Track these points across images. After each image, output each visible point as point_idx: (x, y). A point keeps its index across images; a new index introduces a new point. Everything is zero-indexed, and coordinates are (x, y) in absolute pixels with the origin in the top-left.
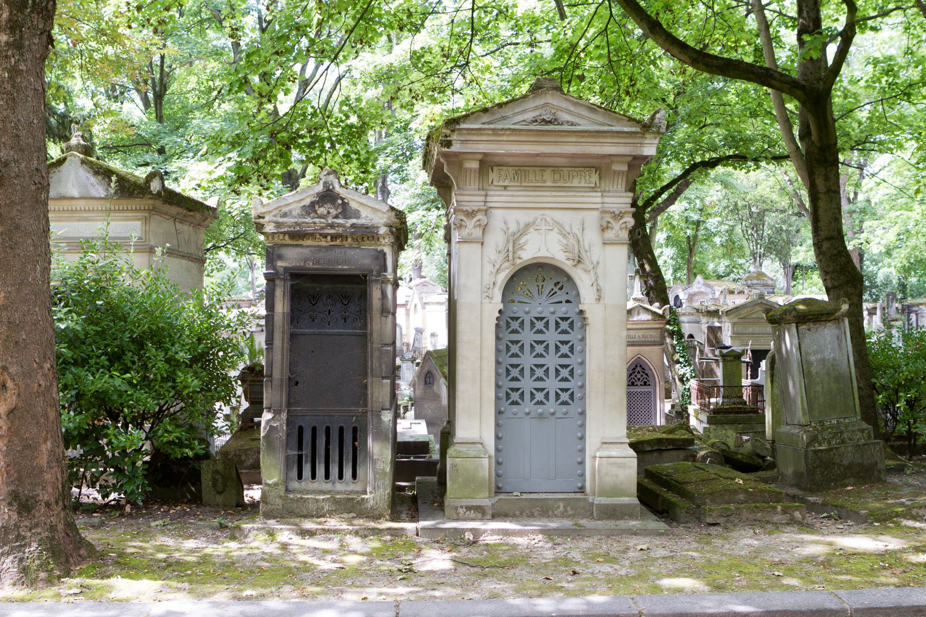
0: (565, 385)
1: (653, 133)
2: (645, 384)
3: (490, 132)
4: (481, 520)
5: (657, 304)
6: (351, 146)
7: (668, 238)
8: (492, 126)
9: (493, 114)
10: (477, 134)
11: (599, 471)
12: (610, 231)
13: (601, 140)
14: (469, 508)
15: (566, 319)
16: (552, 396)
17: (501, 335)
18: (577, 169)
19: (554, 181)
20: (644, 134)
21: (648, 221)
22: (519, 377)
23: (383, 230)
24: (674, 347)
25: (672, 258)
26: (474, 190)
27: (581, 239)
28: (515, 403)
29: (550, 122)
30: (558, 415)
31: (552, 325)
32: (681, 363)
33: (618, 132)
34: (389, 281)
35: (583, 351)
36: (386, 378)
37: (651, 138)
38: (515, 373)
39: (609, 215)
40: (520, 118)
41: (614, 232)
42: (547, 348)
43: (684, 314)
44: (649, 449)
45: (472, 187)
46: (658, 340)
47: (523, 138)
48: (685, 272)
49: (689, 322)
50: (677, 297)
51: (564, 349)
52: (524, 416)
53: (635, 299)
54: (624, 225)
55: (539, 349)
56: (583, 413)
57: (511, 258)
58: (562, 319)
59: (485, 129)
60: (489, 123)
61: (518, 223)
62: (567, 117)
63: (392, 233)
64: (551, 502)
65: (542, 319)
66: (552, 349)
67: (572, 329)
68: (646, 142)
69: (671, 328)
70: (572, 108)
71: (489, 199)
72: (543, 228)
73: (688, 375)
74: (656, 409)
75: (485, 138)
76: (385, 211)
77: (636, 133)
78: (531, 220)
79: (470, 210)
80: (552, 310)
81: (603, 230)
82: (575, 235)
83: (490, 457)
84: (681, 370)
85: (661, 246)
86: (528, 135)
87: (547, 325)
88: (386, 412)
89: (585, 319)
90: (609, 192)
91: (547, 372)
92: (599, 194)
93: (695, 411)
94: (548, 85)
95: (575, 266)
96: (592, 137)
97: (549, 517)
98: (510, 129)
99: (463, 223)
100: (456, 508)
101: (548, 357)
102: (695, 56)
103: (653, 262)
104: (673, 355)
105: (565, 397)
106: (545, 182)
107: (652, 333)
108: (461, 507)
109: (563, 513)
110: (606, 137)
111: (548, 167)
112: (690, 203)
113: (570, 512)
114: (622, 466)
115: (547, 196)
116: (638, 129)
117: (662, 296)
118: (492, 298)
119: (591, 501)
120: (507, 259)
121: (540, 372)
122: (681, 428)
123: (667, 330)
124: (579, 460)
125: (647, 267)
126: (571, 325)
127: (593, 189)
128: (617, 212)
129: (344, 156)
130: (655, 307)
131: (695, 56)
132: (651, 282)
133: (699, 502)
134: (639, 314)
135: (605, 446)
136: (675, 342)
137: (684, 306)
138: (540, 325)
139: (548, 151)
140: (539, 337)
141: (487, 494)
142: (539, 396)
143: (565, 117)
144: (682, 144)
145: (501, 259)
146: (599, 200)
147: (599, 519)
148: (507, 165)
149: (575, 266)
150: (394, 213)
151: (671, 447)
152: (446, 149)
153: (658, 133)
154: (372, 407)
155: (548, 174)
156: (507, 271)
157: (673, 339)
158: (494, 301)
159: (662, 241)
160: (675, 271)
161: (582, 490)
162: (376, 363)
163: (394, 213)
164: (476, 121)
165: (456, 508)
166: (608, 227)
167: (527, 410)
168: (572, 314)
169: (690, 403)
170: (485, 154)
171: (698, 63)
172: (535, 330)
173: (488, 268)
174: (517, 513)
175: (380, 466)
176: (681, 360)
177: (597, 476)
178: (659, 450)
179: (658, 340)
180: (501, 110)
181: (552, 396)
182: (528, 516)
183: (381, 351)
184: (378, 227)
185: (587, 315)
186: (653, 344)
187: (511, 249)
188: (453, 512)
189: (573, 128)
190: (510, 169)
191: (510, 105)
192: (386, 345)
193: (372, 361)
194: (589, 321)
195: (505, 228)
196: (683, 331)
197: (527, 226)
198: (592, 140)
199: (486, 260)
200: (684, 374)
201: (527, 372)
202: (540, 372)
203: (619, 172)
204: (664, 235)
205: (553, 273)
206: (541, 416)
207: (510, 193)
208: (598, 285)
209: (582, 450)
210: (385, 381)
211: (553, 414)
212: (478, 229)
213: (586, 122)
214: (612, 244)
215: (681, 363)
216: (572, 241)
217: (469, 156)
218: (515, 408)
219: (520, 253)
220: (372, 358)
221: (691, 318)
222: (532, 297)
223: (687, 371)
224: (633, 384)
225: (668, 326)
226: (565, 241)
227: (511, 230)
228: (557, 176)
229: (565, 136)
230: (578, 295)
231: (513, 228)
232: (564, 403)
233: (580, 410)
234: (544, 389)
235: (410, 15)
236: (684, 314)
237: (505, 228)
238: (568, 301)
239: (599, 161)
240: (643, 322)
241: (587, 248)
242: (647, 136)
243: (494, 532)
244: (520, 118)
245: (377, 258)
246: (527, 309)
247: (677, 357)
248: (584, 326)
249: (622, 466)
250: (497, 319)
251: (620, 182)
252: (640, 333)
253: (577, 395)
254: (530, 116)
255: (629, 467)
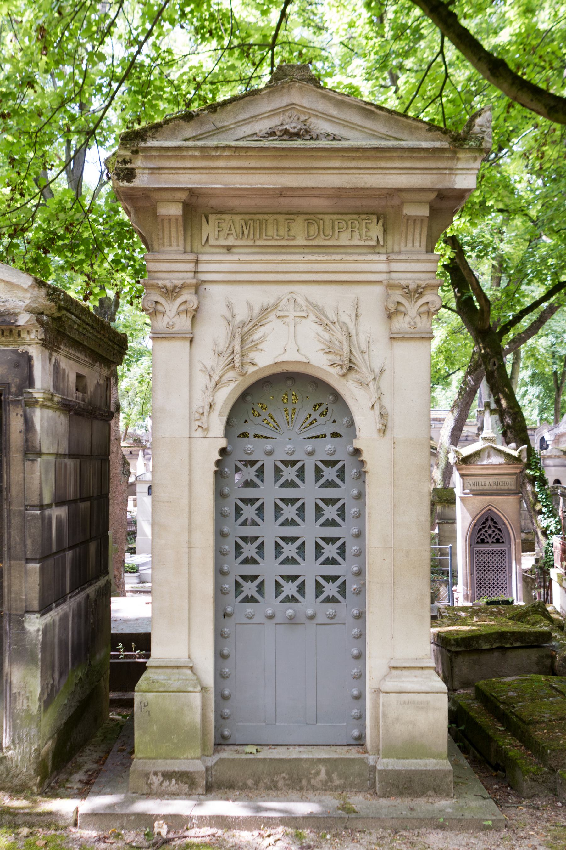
0: (330, 570)
1: (471, 149)
2: (498, 541)
3: (197, 153)
4: (188, 796)
5: (513, 445)
6: (123, 249)
7: (534, 376)
8: (200, 143)
9: (202, 123)
10: (176, 157)
11: (384, 715)
12: (401, 317)
13: (383, 164)
14: (167, 776)
15: (333, 463)
16: (310, 589)
17: (226, 490)
18: (346, 217)
19: (308, 238)
20: (455, 152)
21: (508, 352)
22: (257, 557)
23: (24, 319)
24: (535, 495)
25: (538, 397)
26: (177, 253)
27: (353, 332)
28: (250, 600)
29: (297, 135)
30: (320, 619)
31: (310, 473)
32: (544, 514)
33: (412, 150)
34: (36, 402)
35: (360, 516)
36: (32, 560)
37: (468, 160)
38: (249, 550)
39: (399, 292)
40: (247, 130)
41: (407, 319)
42: (301, 510)
43: (549, 457)
44: (486, 646)
45: (174, 248)
46: (513, 487)
47: (253, 164)
48: (552, 412)
49: (555, 466)
50: (542, 439)
51: (330, 512)
52: (265, 620)
53: (484, 439)
54: (424, 308)
55: (290, 512)
56: (361, 617)
57: (237, 364)
58: (327, 463)
59: (188, 148)
60: (195, 138)
61: (250, 307)
62: (324, 127)
63: (42, 324)
64: (305, 766)
65: (294, 463)
66: (310, 511)
67: (343, 480)
68: (460, 166)
69: (532, 473)
70: (334, 112)
71: (202, 267)
72: (292, 314)
73: (552, 528)
74: (511, 572)
75: (189, 164)
76: (26, 286)
77: (441, 150)
78: (272, 301)
79: (169, 285)
80: (310, 449)
81: (390, 317)
82: (344, 326)
83: (204, 689)
84: (543, 522)
85: (526, 385)
86: (260, 158)
87: (301, 473)
88: (34, 617)
89: (363, 462)
90: (399, 253)
91: (301, 549)
92: (383, 257)
93: (559, 576)
94: (297, 75)
95: (344, 375)
96: (368, 158)
97: (301, 789)
98: (229, 147)
99: (159, 308)
100: (147, 775)
101: (303, 525)
102: (552, 103)
103: (511, 397)
104: (534, 504)
105: (331, 589)
106: (294, 239)
107: (506, 479)
108: (156, 774)
109: (325, 783)
110: (391, 158)
111: (299, 213)
112: (557, 338)
113: (337, 782)
114: (423, 707)
115: (296, 262)
116: (446, 145)
117: (522, 436)
118: (207, 430)
119: (371, 763)
120: (231, 365)
121: (290, 550)
122: (536, 612)
123: (527, 476)
124: (355, 692)
125: (504, 403)
126: (341, 474)
127: (374, 249)
128: (413, 287)
129: (113, 261)
130: (511, 449)
131: (552, 103)
132: (508, 420)
133: (553, 764)
134: (489, 456)
135: (394, 672)
136: (537, 490)
137: (550, 447)
138: (290, 473)
139: (294, 184)
140: (289, 493)
141: (198, 752)
142: (290, 589)
143: (324, 127)
144: (544, 260)
145: (222, 364)
146: (383, 267)
147: (385, 795)
148: (232, 212)
149: (344, 375)
150: (43, 292)
151: (518, 644)
152: (126, 184)
153: (480, 149)
154: (10, 609)
155: (299, 225)
156: (232, 385)
157: (534, 486)
158: (211, 434)
159: (527, 379)
160: (542, 411)
161: (359, 741)
162: (15, 536)
163: (43, 292)
164: (173, 135)
165: (147, 775)
166: (397, 312)
167: (269, 612)
168: (342, 455)
169: (553, 566)
170: (192, 192)
171: (557, 112)
172: (282, 481)
173: (201, 380)
174: (250, 782)
175: (21, 705)
176: (544, 510)
177: (381, 724)
178: (502, 649)
179: (513, 487)
180: (214, 117)
181: (310, 589)
182: (268, 788)
183: (24, 517)
184: (15, 314)
185: (364, 457)
186: (508, 493)
187: (237, 349)
188: (142, 782)
189: (335, 144)
190: (237, 218)
191: (229, 107)
192: (33, 506)
193: (9, 534)
194: (368, 467)
195: (228, 316)
196: (546, 476)
197: (265, 311)
198: (368, 164)
199: (198, 367)
200: (548, 526)
201: (269, 549)
202: (290, 550)
203: (415, 220)
204: (529, 372)
205: (310, 388)
206: (292, 621)
207: (236, 257)
208: (382, 407)
209: (360, 677)
210: (31, 566)
211: (312, 617)
212: (184, 316)
213: (357, 134)
214: (404, 339)
215: (544, 514)
216: (340, 335)
217: (165, 195)
218: (250, 608)
219: (254, 356)
220: (9, 527)
221: (557, 461)
222: (276, 428)
223: (551, 523)
224: (483, 541)
225: (528, 471)
226: (326, 336)
227: (239, 319)
228: (313, 229)
229: (321, 158)
230: (352, 423)
231: (242, 315)
232: (330, 600)
233: (355, 612)
234: (297, 577)
235: (198, 87)
236: (549, 457)
237: (228, 316)
238: (335, 435)
239: (383, 203)
240: (494, 467)
241: (364, 346)
242: (461, 155)
243: (203, 821)
244: (247, 130)
245: (17, 365)
246: (269, 448)
247: (539, 507)
248: (361, 475)
249: (423, 707)
250: (218, 463)
251: (417, 236)
252: (491, 480)
253: (352, 587)
254: (263, 126)
255: (435, 709)
